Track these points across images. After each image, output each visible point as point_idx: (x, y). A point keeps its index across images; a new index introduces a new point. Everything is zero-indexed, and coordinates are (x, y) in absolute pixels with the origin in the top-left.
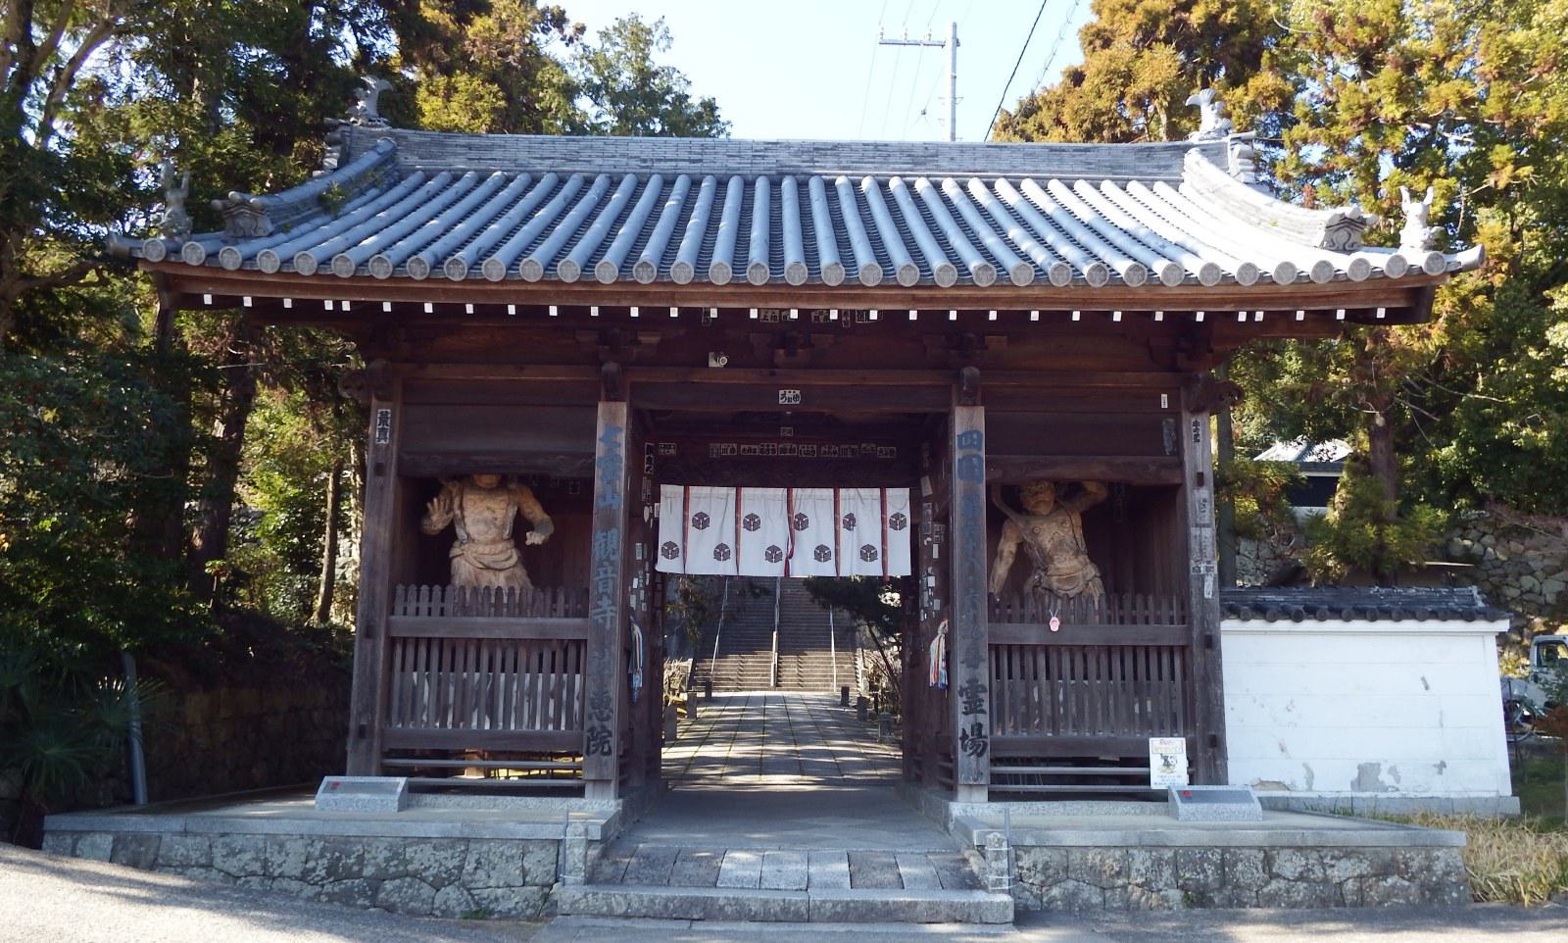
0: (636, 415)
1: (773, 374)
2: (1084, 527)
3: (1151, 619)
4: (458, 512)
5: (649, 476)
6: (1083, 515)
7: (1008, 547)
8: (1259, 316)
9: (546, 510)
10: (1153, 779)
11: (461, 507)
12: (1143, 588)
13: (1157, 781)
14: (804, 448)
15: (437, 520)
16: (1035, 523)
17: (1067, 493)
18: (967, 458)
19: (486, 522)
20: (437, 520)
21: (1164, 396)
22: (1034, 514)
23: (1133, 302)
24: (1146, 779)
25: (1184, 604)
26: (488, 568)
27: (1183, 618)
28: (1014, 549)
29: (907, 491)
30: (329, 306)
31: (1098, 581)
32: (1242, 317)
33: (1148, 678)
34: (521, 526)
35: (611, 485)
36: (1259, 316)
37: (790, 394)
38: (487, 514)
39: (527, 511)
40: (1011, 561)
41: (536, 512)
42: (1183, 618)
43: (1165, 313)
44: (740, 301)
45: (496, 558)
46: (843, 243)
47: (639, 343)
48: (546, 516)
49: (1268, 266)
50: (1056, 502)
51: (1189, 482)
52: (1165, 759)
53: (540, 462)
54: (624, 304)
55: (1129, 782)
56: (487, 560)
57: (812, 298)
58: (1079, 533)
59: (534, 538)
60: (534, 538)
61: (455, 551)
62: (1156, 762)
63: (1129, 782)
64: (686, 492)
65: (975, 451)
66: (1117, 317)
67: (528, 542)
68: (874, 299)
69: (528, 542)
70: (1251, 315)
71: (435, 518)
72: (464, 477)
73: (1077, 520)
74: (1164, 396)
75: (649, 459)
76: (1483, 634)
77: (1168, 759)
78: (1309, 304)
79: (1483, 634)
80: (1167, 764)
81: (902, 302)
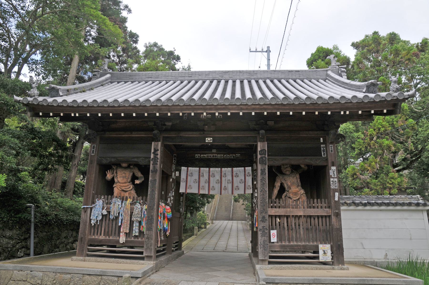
0: (165, 147)
1: (204, 133)
2: (300, 178)
3: (319, 207)
4: (115, 174)
5: (174, 164)
6: (300, 174)
7: (278, 185)
8: (348, 113)
9: (142, 173)
10: (320, 258)
11: (116, 173)
12: (319, 197)
13: (322, 259)
14: (219, 156)
15: (109, 176)
16: (286, 177)
17: (295, 168)
18: (261, 158)
19: (123, 177)
20: (109, 176)
21: (322, 139)
22: (285, 174)
23: (309, 109)
24: (318, 258)
25: (329, 203)
26: (123, 191)
27: (329, 206)
28: (279, 185)
29: (251, 168)
30: (73, 115)
31: (304, 195)
32: (342, 113)
33: (319, 225)
34: (134, 178)
35: (156, 166)
36: (348, 113)
37: (209, 139)
38: (124, 175)
39: (136, 174)
40: (278, 188)
41: (139, 174)
42: (329, 206)
43: (243, 113)
44: (189, 111)
45: (126, 187)
46: (270, 90)
47: (166, 125)
48: (142, 175)
49: (338, 97)
50: (292, 171)
51: (330, 164)
52: (324, 251)
53: (136, 160)
54: (154, 112)
55: (314, 258)
56: (123, 188)
57: (210, 109)
58: (299, 180)
59: (137, 182)
60: (137, 182)
61: (114, 186)
62: (329, 252)
63: (314, 258)
64: (188, 169)
65: (263, 156)
66: (317, 113)
67: (135, 183)
68: (229, 109)
69: (135, 183)
70: (345, 112)
71: (108, 176)
72: (116, 165)
73: (298, 176)
74: (322, 139)
75: (175, 159)
76: (422, 211)
77: (325, 251)
78: (256, 110)
79: (422, 211)
80: (325, 253)
81: (238, 110)
